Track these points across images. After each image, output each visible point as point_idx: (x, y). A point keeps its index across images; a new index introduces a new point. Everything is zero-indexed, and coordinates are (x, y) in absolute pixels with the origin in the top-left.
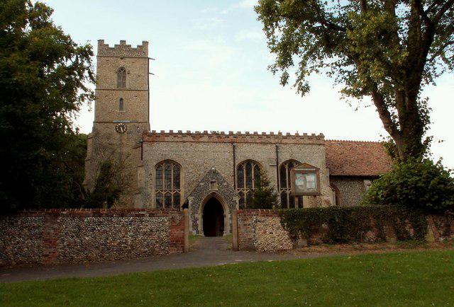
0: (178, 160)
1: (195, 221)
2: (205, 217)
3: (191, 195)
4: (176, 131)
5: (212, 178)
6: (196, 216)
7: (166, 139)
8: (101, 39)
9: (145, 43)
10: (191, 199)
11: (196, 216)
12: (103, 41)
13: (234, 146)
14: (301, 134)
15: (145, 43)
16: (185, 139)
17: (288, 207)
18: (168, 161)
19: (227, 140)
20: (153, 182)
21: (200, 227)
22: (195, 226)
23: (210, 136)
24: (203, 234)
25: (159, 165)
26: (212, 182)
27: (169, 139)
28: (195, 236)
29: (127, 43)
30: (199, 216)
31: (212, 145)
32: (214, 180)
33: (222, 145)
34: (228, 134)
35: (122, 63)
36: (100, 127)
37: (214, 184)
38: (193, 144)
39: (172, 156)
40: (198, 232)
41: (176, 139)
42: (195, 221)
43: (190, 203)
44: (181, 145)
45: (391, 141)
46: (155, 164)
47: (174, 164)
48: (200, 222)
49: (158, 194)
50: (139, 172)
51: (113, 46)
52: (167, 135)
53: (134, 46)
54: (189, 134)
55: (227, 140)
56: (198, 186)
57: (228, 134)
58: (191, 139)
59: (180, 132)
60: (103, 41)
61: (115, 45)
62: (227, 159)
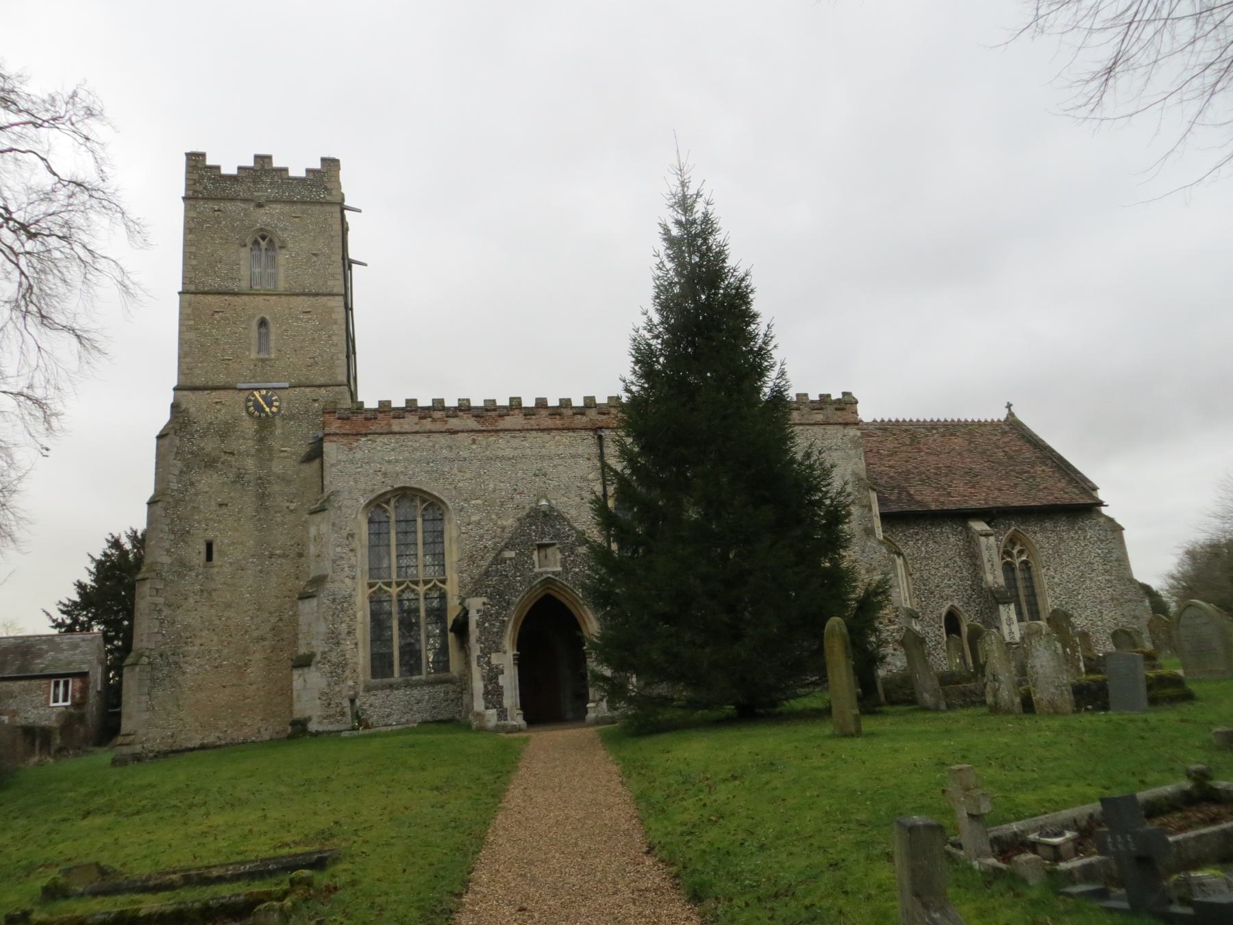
0: (434, 488)
1: (492, 676)
2: (523, 663)
3: (475, 593)
4: (425, 401)
5: (543, 534)
6: (495, 659)
7: (396, 426)
8: (200, 150)
9: (331, 165)
10: (476, 604)
11: (495, 659)
12: (270, 157)
13: (600, 438)
14: (528, 402)
15: (331, 165)
16: (454, 423)
17: (396, 674)
18: (405, 494)
19: (581, 421)
20: (361, 559)
21: (511, 698)
22: (494, 695)
23: (528, 413)
24: (519, 721)
25: (377, 504)
26: (541, 547)
27: (409, 423)
28: (498, 729)
29: (276, 163)
30: (506, 658)
31: (535, 438)
32: (546, 541)
33: (566, 437)
34: (507, 403)
35: (263, 217)
36: (192, 401)
37: (550, 551)
38: (480, 437)
39: (421, 480)
40: (502, 714)
41: (427, 424)
42: (492, 676)
43: (474, 617)
44: (443, 440)
45: (762, 402)
46: (363, 501)
47: (423, 501)
48: (509, 681)
49: (376, 600)
50: (313, 531)
51: (234, 172)
52: (400, 413)
53: (297, 171)
54: (465, 407)
55: (581, 421)
56: (498, 560)
57: (581, 404)
58: (472, 423)
59: (438, 405)
60: (270, 157)
61: (308, 171)
62: (584, 479)
